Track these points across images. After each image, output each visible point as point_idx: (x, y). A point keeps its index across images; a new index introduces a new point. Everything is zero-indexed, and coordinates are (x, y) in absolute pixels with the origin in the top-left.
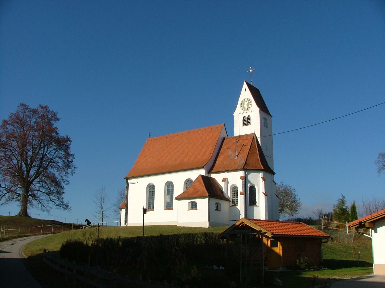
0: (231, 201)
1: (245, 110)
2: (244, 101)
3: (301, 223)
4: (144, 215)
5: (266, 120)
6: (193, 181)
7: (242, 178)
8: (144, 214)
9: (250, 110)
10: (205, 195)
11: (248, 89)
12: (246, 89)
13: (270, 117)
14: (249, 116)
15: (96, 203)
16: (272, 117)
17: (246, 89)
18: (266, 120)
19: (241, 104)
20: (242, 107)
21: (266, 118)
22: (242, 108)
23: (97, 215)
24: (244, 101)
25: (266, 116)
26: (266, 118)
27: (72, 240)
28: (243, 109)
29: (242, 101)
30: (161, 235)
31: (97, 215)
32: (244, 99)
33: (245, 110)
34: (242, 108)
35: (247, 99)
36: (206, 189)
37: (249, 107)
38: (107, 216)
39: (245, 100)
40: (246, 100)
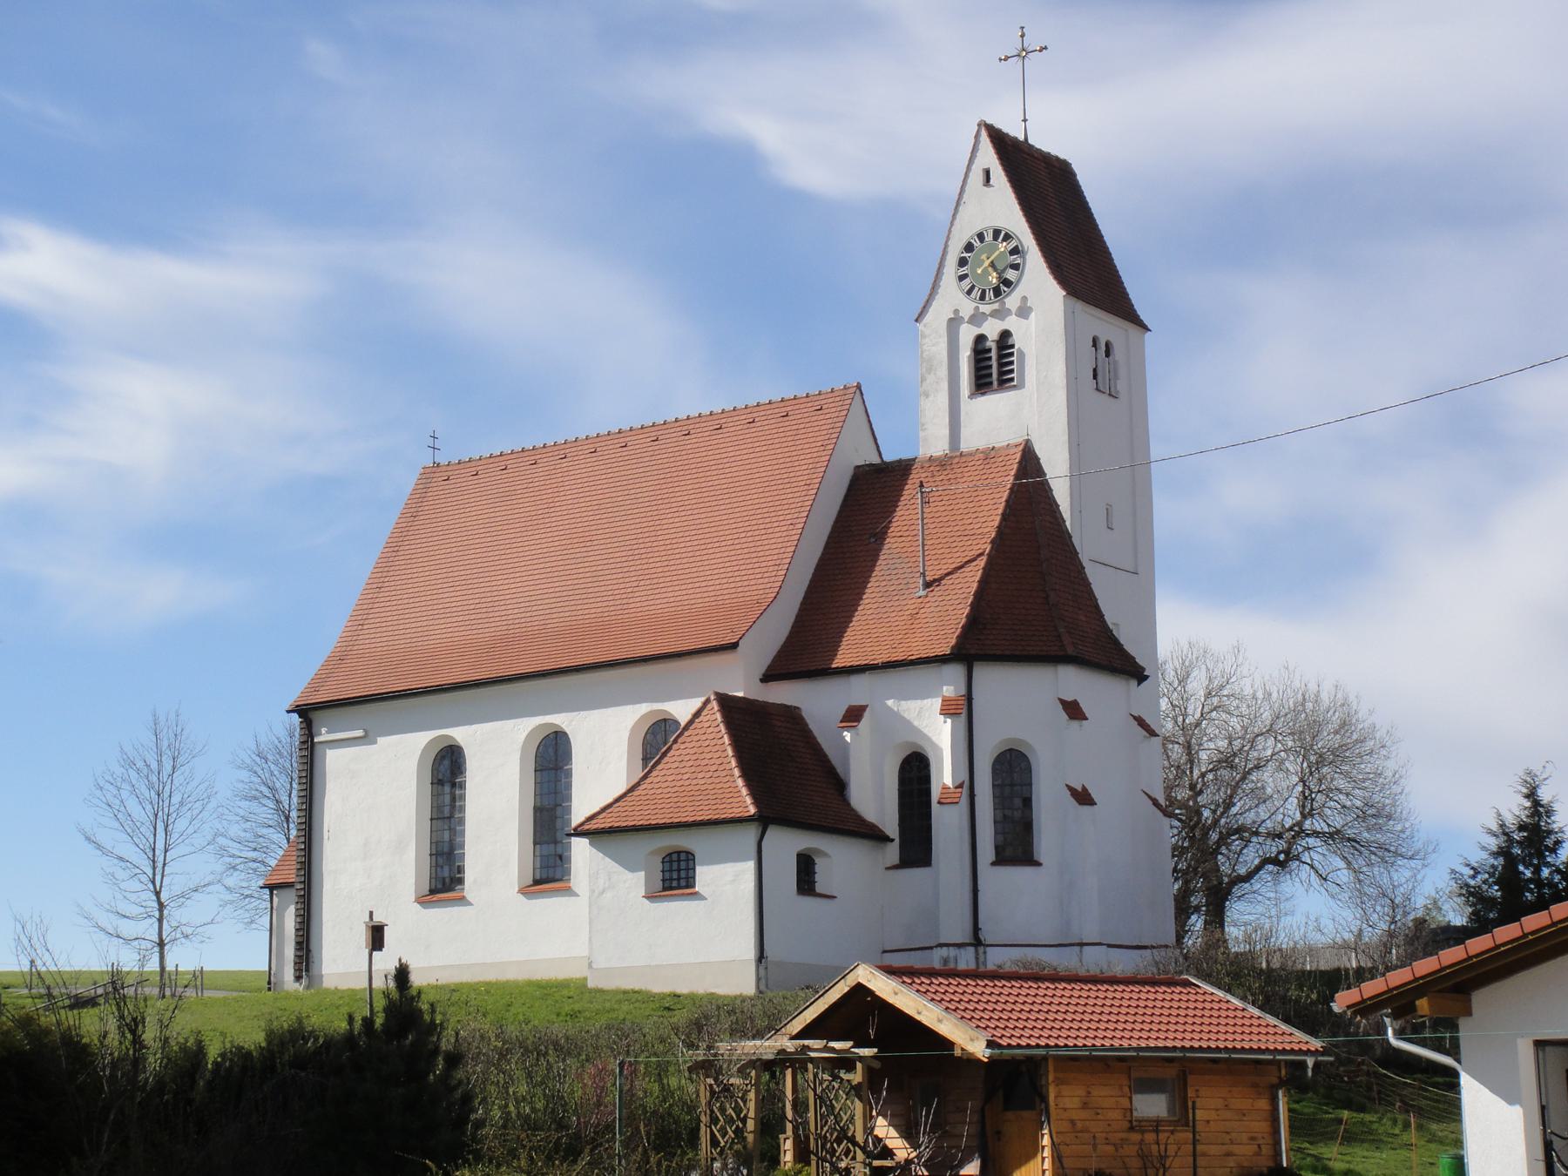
0: (892, 840)
1: (982, 297)
2: (977, 244)
3: (1187, 984)
4: (371, 955)
5: (1108, 354)
6: (676, 723)
7: (948, 710)
8: (374, 953)
9: (1012, 301)
10: (736, 812)
11: (999, 175)
12: (987, 173)
13: (1132, 330)
14: (1005, 335)
15: (121, 859)
16: (1146, 328)
17: (987, 173)
18: (1108, 354)
19: (963, 262)
20: (967, 281)
21: (1108, 345)
22: (966, 284)
23: (128, 928)
24: (977, 244)
25: (1107, 326)
26: (1108, 345)
27: (1387, 758)
28: (969, 292)
29: (969, 247)
30: (336, 988)
31: (128, 928)
32: (977, 229)
33: (982, 297)
34: (966, 284)
35: (997, 233)
36: (747, 774)
37: (1007, 283)
38: (189, 930)
39: (981, 236)
40: (989, 237)
